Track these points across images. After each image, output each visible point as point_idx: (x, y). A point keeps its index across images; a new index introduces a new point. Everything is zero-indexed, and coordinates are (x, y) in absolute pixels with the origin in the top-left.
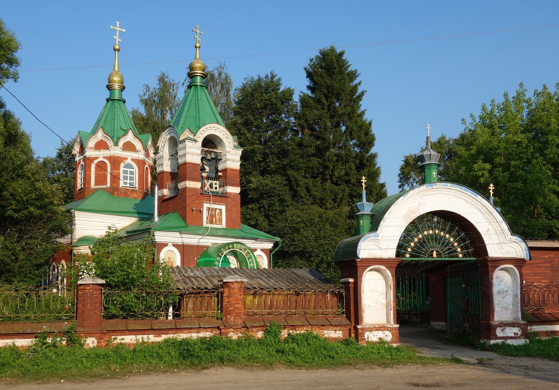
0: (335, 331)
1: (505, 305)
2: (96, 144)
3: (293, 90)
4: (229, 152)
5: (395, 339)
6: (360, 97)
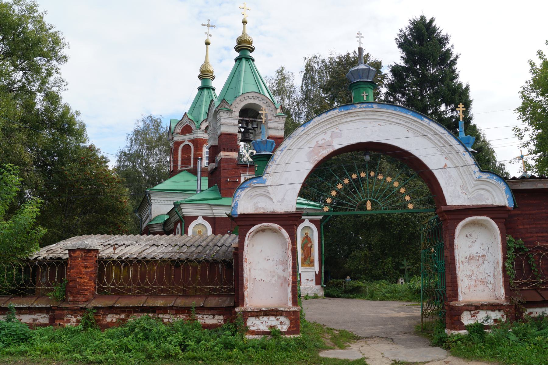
0: (214, 315)
1: (481, 277)
2: (183, 129)
3: (381, 62)
4: (270, 120)
5: (293, 327)
6: (454, 62)
